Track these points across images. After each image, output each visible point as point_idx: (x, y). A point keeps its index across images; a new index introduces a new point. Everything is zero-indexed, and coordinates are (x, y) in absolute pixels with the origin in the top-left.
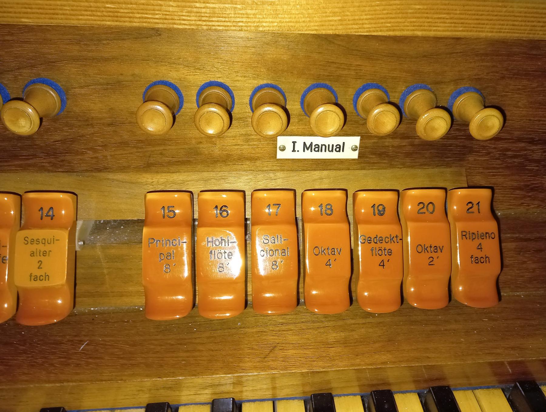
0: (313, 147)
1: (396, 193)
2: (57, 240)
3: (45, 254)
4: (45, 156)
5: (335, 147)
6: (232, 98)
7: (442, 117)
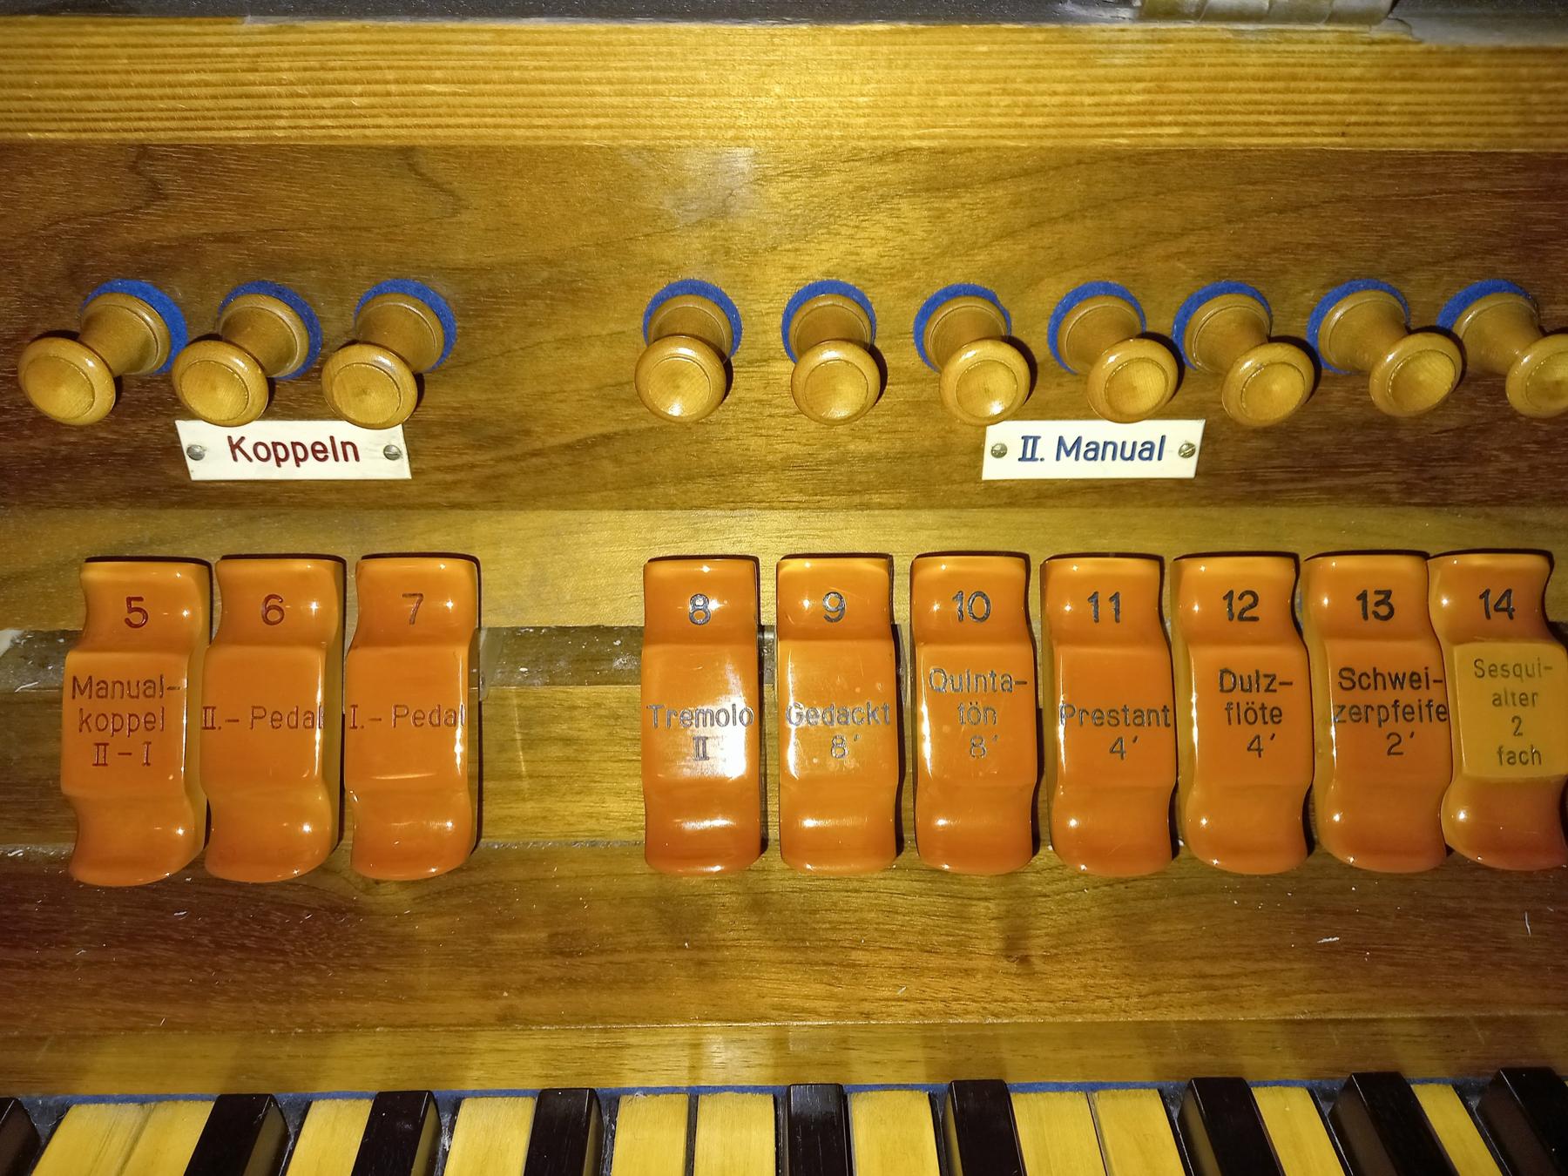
0: (1083, 449)
1: (1289, 562)
2: (1546, 668)
3: (1524, 700)
4: (1399, 466)
5: (1139, 448)
6: (872, 322)
7: (1284, 363)
